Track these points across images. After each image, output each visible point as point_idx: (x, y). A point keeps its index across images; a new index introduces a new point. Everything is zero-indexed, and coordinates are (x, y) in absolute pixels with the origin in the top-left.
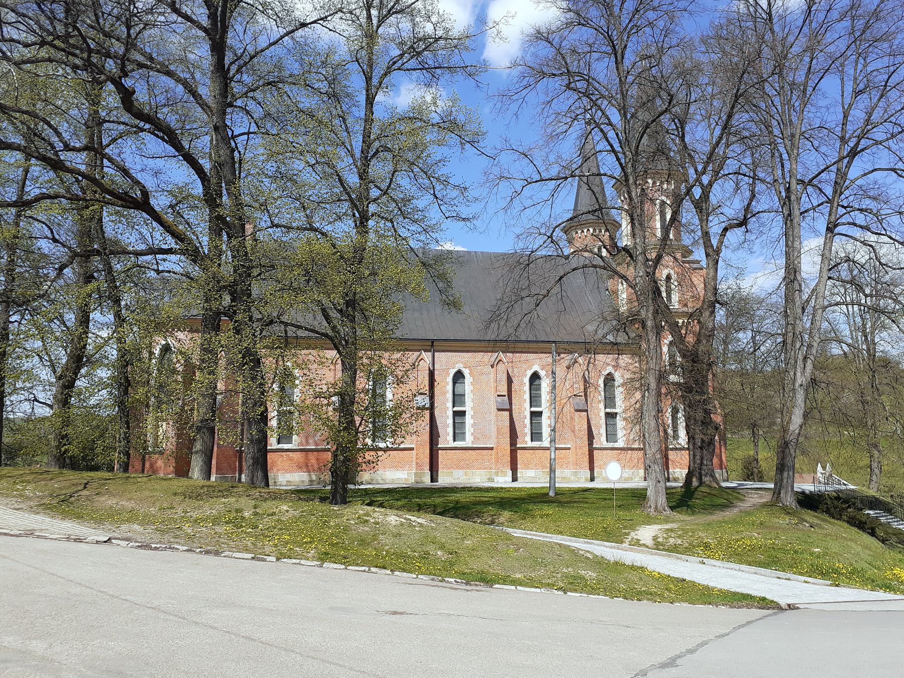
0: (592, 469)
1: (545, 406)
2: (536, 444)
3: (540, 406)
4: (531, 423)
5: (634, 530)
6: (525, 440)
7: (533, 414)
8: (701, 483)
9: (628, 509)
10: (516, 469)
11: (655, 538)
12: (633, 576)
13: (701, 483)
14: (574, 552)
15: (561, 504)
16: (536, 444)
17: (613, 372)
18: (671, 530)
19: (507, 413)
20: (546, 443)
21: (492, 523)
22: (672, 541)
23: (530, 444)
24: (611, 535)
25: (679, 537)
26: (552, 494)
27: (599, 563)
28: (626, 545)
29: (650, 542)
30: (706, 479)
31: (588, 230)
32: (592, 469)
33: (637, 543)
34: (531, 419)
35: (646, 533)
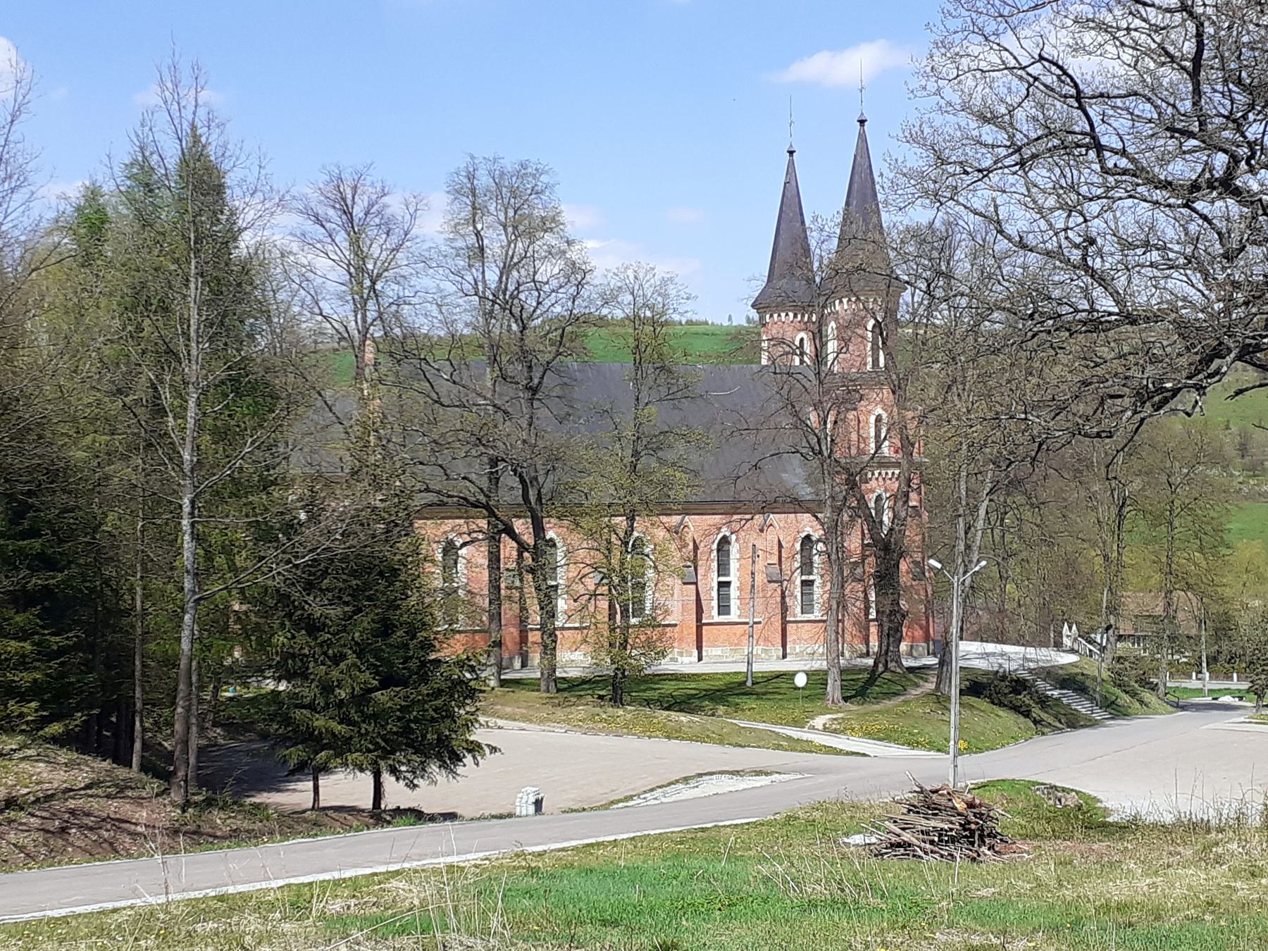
0: (784, 645)
1: (733, 578)
2: (723, 618)
3: (728, 575)
4: (719, 595)
5: (813, 719)
6: (712, 614)
7: (721, 584)
8: (886, 669)
9: (812, 701)
10: (701, 647)
11: (824, 725)
12: (805, 745)
13: (886, 669)
14: (777, 734)
15: (759, 695)
16: (723, 618)
17: (811, 533)
18: (835, 719)
19: (693, 587)
20: (734, 616)
21: (713, 715)
22: (834, 726)
23: (717, 619)
24: (798, 723)
25: (840, 724)
26: (749, 684)
27: (790, 738)
28: (806, 729)
29: (821, 727)
30: (892, 665)
31: (787, 315)
32: (784, 645)
33: (813, 728)
34: (718, 590)
35: (819, 721)
